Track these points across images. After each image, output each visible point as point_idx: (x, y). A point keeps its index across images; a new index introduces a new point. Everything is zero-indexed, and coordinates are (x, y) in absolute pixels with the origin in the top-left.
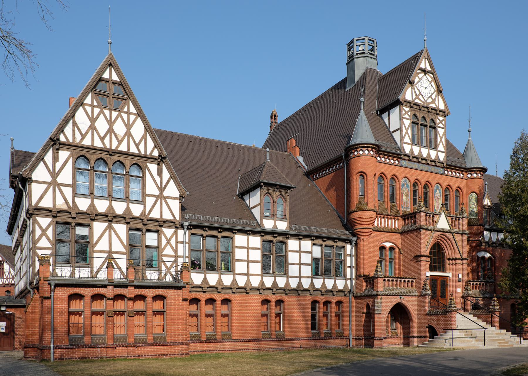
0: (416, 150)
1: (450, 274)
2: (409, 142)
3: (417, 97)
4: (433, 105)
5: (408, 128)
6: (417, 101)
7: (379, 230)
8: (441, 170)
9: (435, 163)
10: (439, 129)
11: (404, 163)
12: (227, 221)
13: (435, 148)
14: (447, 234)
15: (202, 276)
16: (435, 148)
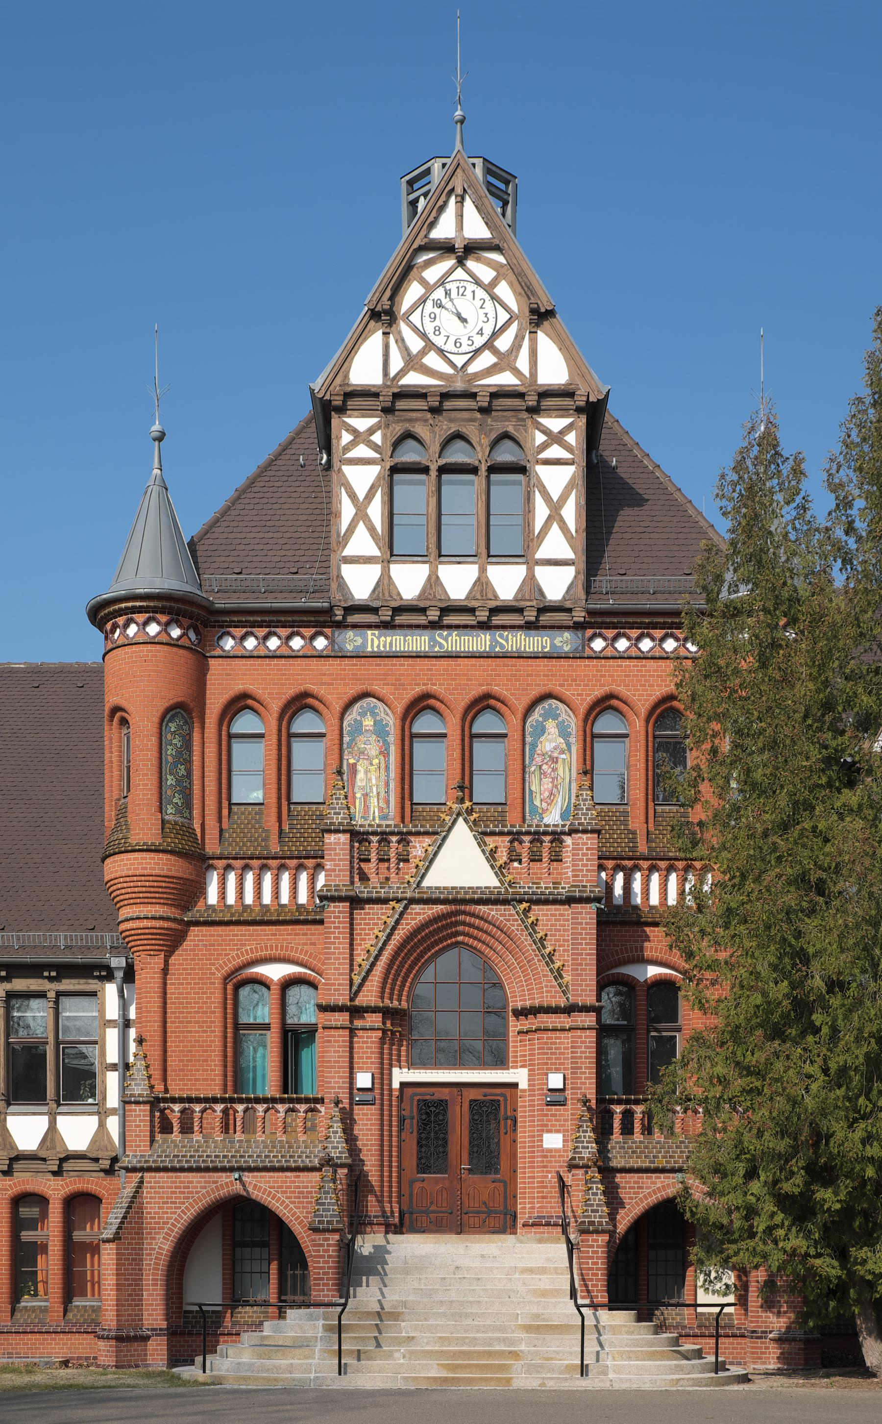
0: (409, 581)
1: (519, 1076)
2: (372, 549)
3: (413, 362)
4: (506, 379)
5: (370, 496)
6: (413, 379)
7: (246, 917)
8: (565, 641)
9: (534, 613)
10: (540, 469)
11: (351, 640)
12: (61, 942)
13: (524, 553)
14: (482, 909)
15: (42, 1122)
16: (524, 553)
